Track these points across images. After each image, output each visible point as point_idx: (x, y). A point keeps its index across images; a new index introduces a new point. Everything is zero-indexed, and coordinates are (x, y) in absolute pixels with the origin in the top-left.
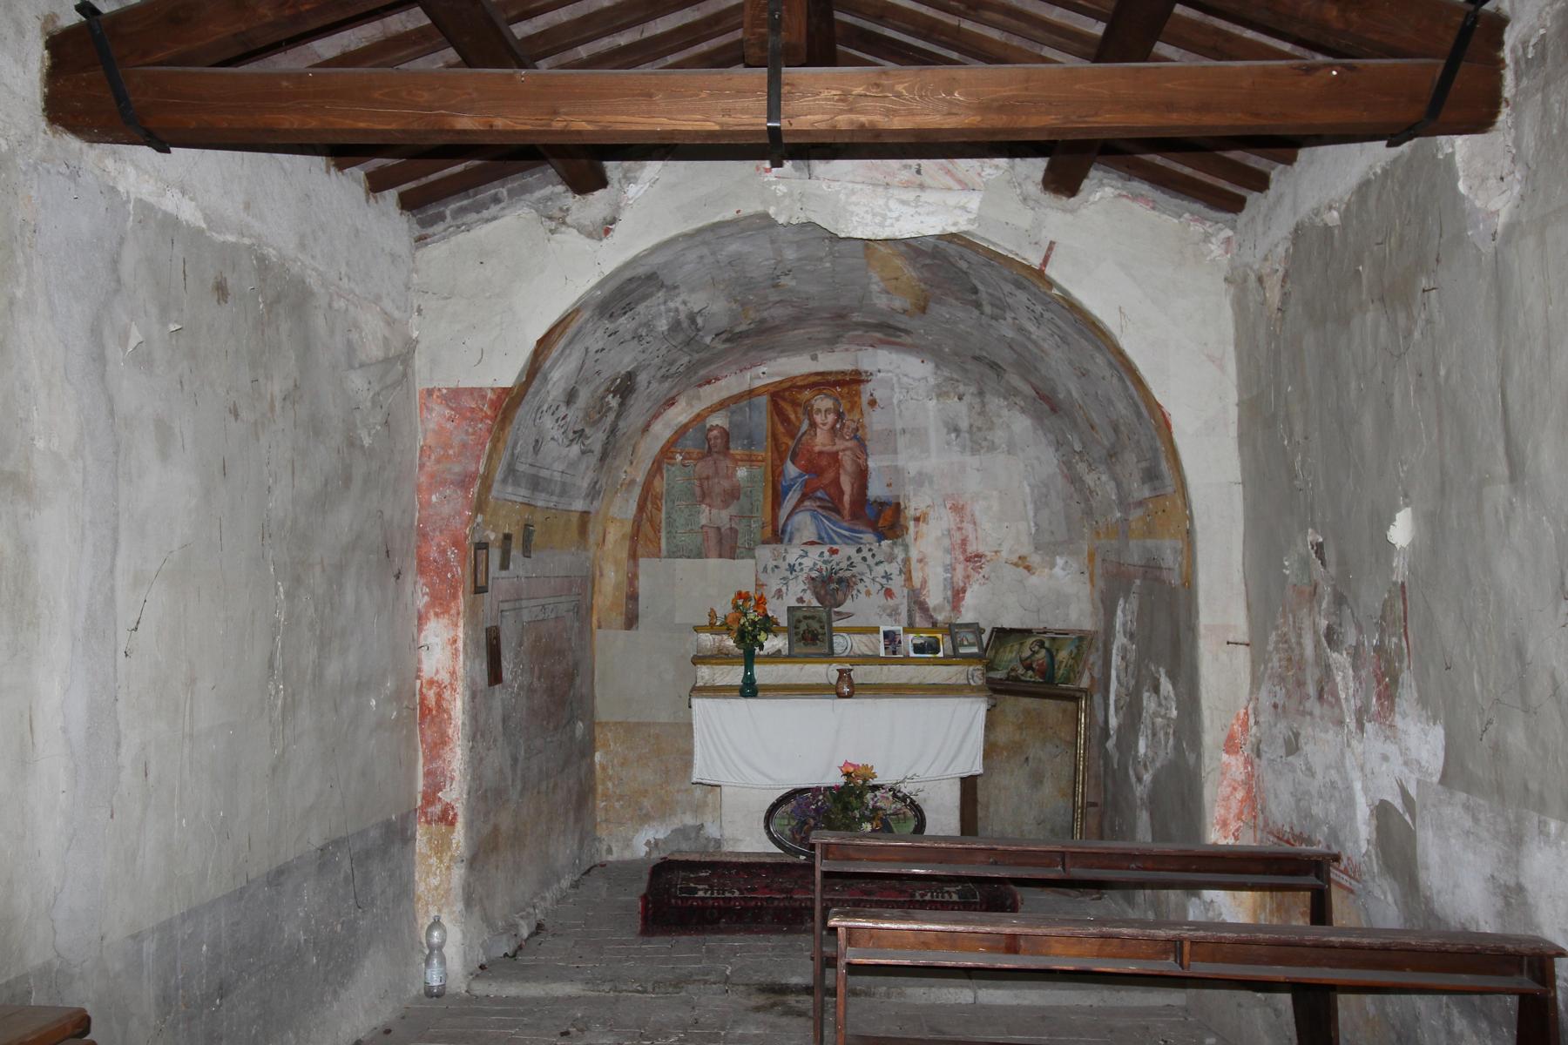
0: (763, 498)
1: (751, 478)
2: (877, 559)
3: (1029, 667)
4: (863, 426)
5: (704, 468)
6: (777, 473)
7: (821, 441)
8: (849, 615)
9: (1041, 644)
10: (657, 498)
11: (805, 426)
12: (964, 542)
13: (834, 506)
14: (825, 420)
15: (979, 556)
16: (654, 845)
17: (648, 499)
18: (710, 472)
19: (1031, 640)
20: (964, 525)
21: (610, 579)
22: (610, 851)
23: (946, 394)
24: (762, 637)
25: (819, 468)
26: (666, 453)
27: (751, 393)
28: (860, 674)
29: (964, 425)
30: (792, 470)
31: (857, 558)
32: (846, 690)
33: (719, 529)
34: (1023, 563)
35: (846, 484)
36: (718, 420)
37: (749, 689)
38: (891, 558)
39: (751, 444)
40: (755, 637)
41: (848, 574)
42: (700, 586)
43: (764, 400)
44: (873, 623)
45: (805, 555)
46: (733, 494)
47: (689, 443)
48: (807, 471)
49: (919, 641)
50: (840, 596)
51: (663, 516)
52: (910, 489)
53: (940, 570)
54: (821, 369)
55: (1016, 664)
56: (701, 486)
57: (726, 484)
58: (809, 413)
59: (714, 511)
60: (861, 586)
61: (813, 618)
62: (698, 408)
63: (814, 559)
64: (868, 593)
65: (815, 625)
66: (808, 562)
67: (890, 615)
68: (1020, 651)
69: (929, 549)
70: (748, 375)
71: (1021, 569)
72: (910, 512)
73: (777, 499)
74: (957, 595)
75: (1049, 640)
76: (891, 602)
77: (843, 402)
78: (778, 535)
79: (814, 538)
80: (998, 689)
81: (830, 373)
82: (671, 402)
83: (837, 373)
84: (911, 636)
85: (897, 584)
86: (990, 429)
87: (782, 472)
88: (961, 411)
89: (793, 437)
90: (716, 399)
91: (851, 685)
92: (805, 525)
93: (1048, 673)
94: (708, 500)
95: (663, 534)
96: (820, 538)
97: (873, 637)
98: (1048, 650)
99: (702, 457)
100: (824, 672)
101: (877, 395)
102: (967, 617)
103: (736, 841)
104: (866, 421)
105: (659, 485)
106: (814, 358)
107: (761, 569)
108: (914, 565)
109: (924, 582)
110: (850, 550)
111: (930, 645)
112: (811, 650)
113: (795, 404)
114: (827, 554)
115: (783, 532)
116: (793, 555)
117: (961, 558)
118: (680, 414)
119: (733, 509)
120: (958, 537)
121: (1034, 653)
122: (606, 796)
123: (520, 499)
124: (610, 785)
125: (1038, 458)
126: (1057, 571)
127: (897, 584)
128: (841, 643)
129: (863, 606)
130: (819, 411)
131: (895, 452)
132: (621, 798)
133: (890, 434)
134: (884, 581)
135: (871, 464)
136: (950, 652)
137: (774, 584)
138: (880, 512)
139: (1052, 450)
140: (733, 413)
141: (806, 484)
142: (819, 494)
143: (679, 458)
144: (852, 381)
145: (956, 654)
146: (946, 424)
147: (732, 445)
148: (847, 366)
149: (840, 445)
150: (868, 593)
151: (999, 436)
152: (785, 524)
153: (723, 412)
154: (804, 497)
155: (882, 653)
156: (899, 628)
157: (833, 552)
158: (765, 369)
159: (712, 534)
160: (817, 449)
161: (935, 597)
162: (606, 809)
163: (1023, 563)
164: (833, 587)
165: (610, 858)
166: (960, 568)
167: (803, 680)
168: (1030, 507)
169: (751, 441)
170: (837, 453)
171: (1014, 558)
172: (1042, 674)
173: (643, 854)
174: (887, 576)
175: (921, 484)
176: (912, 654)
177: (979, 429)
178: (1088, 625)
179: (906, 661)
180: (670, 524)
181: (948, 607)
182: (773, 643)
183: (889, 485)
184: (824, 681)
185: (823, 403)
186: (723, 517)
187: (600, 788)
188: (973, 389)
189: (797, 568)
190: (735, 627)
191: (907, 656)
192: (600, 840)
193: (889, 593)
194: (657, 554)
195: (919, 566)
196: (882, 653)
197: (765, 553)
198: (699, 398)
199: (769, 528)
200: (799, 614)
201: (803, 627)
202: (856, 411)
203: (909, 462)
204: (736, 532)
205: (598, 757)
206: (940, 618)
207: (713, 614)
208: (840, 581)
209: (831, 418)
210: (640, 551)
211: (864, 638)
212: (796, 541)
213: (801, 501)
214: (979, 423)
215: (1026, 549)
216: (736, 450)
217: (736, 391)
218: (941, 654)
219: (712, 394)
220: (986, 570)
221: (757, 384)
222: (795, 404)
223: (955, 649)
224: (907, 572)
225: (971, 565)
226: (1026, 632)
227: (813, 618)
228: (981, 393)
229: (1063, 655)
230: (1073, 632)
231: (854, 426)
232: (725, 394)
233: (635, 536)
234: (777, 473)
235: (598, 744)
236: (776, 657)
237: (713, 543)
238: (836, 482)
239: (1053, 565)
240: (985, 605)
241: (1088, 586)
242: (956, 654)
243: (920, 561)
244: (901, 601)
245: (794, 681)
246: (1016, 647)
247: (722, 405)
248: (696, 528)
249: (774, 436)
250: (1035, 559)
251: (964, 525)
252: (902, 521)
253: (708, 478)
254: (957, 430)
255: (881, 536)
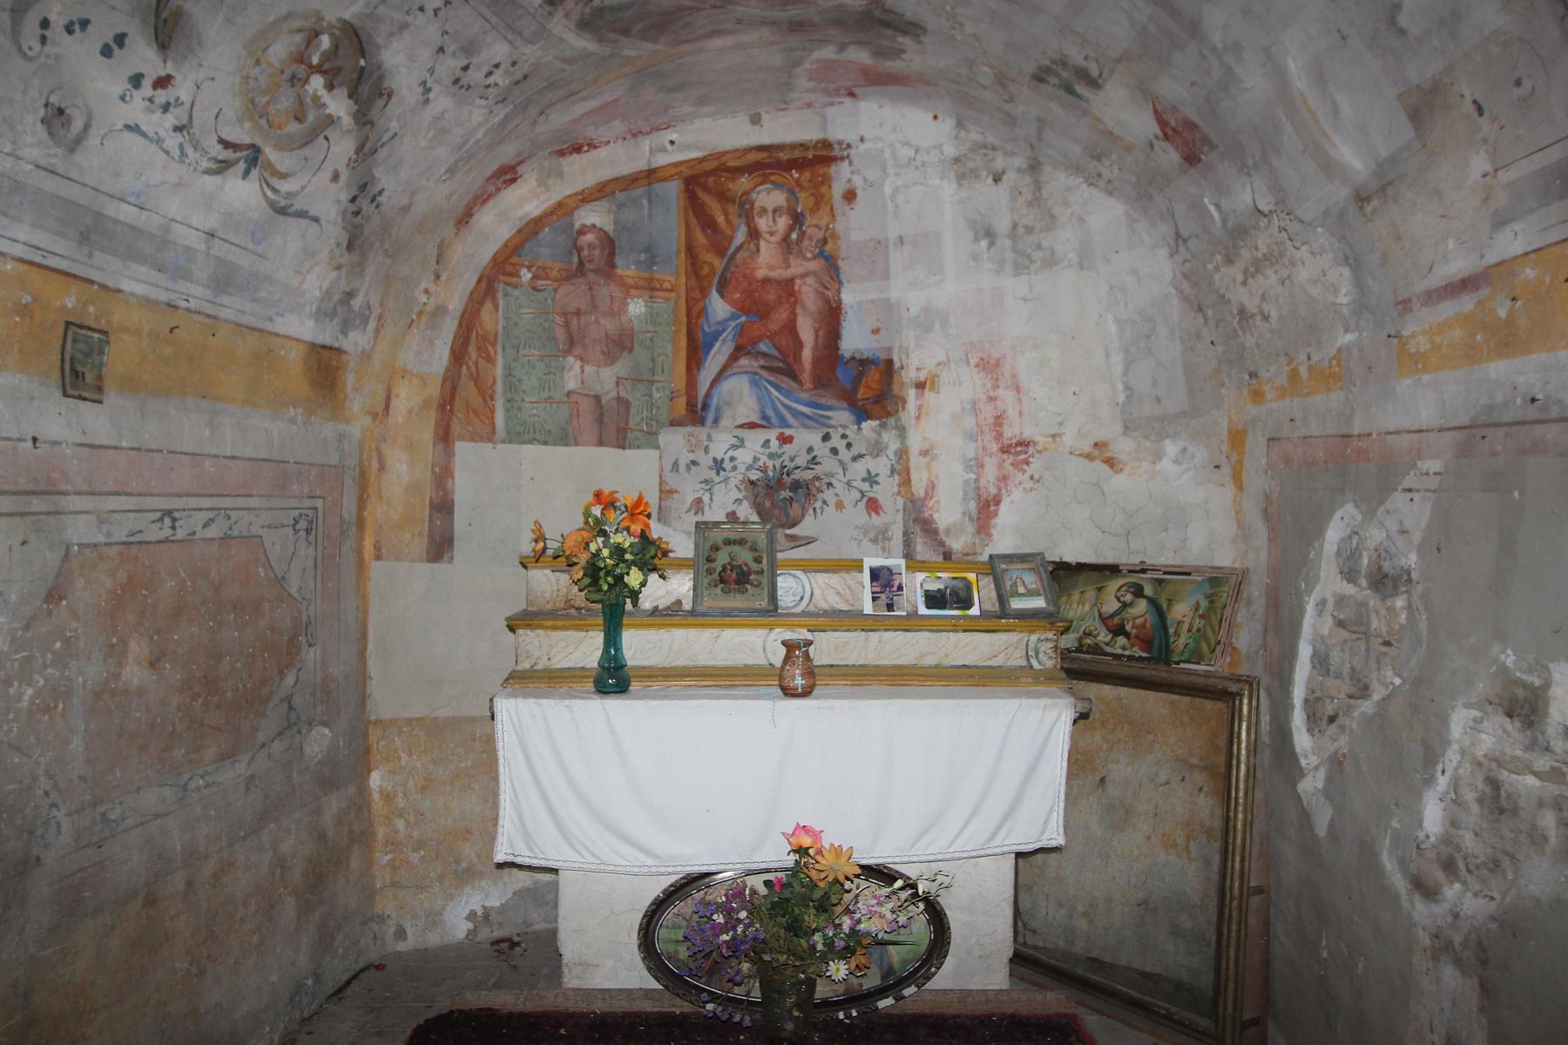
0: (671, 351)
1: (652, 317)
2: (855, 451)
3: (1118, 631)
4: (835, 236)
5: (572, 295)
6: (694, 313)
7: (767, 261)
8: (810, 541)
9: (1138, 592)
10: (488, 340)
11: (741, 235)
12: (999, 421)
13: (786, 367)
14: (773, 226)
15: (1025, 443)
16: (485, 917)
17: (469, 340)
18: (583, 303)
19: (1114, 585)
20: (1000, 392)
21: (402, 474)
22: (401, 934)
23: (974, 174)
24: (634, 578)
25: (762, 304)
26: (503, 266)
27: (651, 176)
28: (828, 648)
29: (1002, 224)
30: (719, 307)
31: (822, 450)
32: (799, 681)
33: (597, 398)
34: (1101, 453)
35: (807, 331)
36: (594, 216)
37: (613, 678)
38: (877, 450)
39: (652, 261)
40: (619, 579)
41: (808, 475)
42: (533, 489)
43: (673, 189)
44: (850, 551)
45: (740, 444)
46: (620, 344)
47: (546, 249)
48: (744, 310)
49: (934, 586)
50: (795, 510)
51: (499, 371)
52: (909, 337)
53: (958, 468)
54: (766, 140)
55: (1093, 623)
56: (567, 326)
57: (609, 325)
58: (748, 214)
59: (589, 369)
60: (828, 495)
61: (741, 542)
62: (560, 191)
63: (753, 452)
64: (840, 506)
65: (744, 556)
66: (744, 456)
67: (875, 541)
68: (1098, 602)
69: (940, 433)
70: (646, 144)
71: (1098, 465)
72: (910, 375)
73: (696, 352)
74: (986, 509)
75: (1154, 584)
76: (876, 520)
77: (802, 195)
78: (696, 412)
79: (755, 418)
80: (1079, 668)
81: (781, 147)
82: (508, 175)
83: (793, 146)
84: (921, 576)
85: (887, 491)
86: (1048, 229)
87: (703, 311)
88: (996, 202)
89: (721, 253)
90: (590, 180)
91: (810, 672)
92: (740, 395)
93: (1157, 643)
94: (578, 350)
95: (499, 405)
96: (765, 417)
97: (849, 578)
98: (1152, 601)
99: (568, 278)
100: (758, 645)
101: (858, 182)
102: (1004, 541)
103: (586, 966)
104: (839, 226)
105: (489, 318)
106: (756, 120)
107: (668, 466)
108: (915, 461)
109: (931, 488)
110: (811, 438)
111: (955, 593)
112: (736, 601)
113: (724, 197)
114: (774, 443)
115: (705, 407)
116: (721, 444)
117: (994, 447)
118: (526, 200)
119: (621, 367)
120: (988, 412)
121: (1125, 605)
122: (393, 844)
123: (18, 250)
124: (400, 824)
125: (1135, 272)
126: (1166, 464)
127: (887, 491)
128: (790, 588)
129: (831, 525)
130: (764, 211)
131: (886, 275)
132: (421, 844)
133: (880, 244)
134: (865, 486)
135: (847, 297)
136: (992, 605)
137: (689, 489)
138: (861, 374)
139: (1163, 253)
140: (621, 206)
141: (741, 331)
142: (763, 347)
143: (526, 275)
144: (812, 163)
145: (1004, 612)
146: (972, 224)
147: (619, 261)
148: (810, 134)
149: (797, 267)
150: (840, 506)
151: (1065, 240)
152: (708, 395)
153: (603, 204)
154: (739, 351)
155: (868, 608)
156: (898, 563)
157: (785, 440)
158: (674, 137)
159: (586, 406)
160: (760, 274)
161: (949, 512)
162: (393, 866)
163: (1101, 453)
164: (783, 496)
165: (402, 947)
166: (991, 464)
167: (722, 659)
168: (1117, 359)
169: (651, 256)
170: (792, 280)
171: (1087, 447)
172: (1147, 644)
173: (461, 935)
174: (871, 479)
175: (928, 329)
176: (923, 610)
177: (1029, 230)
178: (1225, 558)
179: (912, 622)
180: (511, 384)
181: (970, 528)
182: (659, 590)
183: (876, 331)
184: (760, 660)
185: (770, 197)
186: (605, 379)
187: (381, 832)
188: (1020, 161)
189: (727, 465)
190: (583, 558)
191: (913, 615)
192: (382, 919)
193: (873, 506)
194: (490, 437)
195: (923, 461)
196: (868, 608)
197: (675, 441)
198: (560, 174)
199: (682, 402)
200: (717, 536)
201: (722, 558)
202: (825, 210)
203: (910, 291)
204: (627, 404)
205: (376, 779)
206: (956, 544)
207: (540, 537)
208: (796, 486)
209: (783, 222)
210: (456, 428)
211: (834, 579)
212: (726, 422)
213: (734, 357)
214: (1028, 220)
215: (1109, 429)
216: (627, 269)
217: (625, 169)
218: (975, 611)
219: (583, 172)
220: (1035, 467)
221: (661, 160)
222: (724, 197)
223: (1002, 600)
224: (902, 472)
225: (1010, 459)
226: (1114, 570)
227: (741, 542)
228: (1034, 167)
229: (1181, 611)
230: (1199, 570)
231: (819, 235)
232: (606, 174)
233: (447, 403)
234: (694, 313)
235: (375, 757)
236: (669, 615)
237: (587, 419)
238: (791, 328)
239: (1158, 456)
240: (1044, 518)
241: (1229, 492)
242: (1004, 612)
243: (925, 453)
244: (893, 516)
245: (704, 660)
246: (1091, 593)
247: (601, 192)
248: (558, 395)
249: (691, 250)
250: (1123, 447)
251: (1000, 392)
252: (895, 388)
253: (578, 313)
254: (990, 234)
255: (862, 414)
